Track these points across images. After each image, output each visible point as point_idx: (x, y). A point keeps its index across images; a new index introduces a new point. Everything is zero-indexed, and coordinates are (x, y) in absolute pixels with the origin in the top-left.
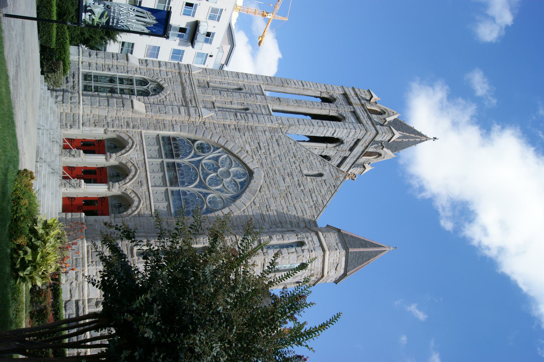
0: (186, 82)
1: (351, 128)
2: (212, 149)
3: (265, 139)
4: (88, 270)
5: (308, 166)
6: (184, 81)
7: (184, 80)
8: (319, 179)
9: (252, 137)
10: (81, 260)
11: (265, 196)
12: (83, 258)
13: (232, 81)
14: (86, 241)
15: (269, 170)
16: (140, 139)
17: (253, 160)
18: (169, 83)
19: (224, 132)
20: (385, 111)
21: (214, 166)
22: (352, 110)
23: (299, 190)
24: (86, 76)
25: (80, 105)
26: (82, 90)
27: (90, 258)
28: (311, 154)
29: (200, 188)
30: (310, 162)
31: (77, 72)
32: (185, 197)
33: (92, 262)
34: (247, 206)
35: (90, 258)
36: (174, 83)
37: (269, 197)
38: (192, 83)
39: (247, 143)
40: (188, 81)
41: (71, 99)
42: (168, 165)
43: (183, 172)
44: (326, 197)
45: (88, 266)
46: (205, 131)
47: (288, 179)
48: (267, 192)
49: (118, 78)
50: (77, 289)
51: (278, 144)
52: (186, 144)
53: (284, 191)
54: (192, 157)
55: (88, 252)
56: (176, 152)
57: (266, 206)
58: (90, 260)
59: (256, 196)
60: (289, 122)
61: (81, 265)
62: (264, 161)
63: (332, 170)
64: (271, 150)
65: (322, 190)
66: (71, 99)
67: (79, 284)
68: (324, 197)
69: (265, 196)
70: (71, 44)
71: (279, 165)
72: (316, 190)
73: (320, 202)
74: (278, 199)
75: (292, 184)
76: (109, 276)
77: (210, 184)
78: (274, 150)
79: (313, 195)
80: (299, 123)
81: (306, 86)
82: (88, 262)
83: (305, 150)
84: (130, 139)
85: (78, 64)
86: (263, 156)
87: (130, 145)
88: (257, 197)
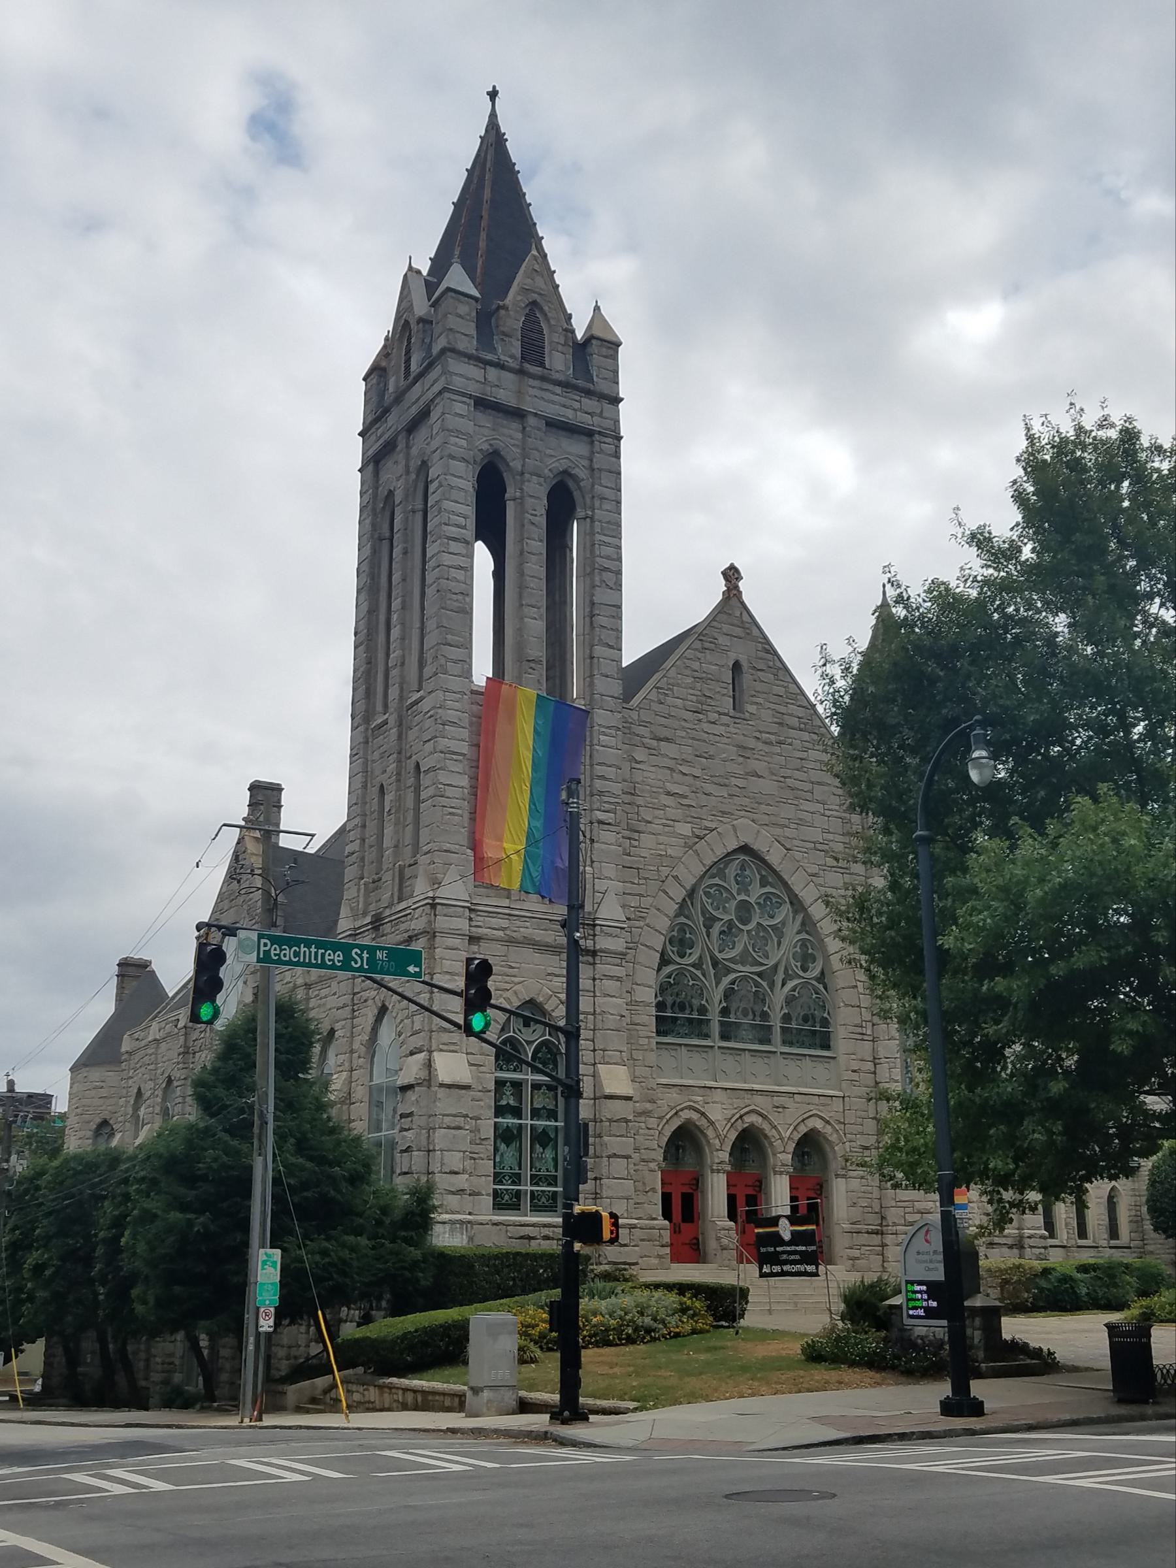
0: (503, 929)
2: (683, 920)
6: (501, 933)
7: (495, 932)
8: (747, 678)
16: (676, 1089)
18: (516, 980)
21: (724, 931)
22: (404, 433)
24: (499, 1204)
32: (669, 1006)
36: (513, 965)
38: (507, 911)
42: (725, 1037)
46: (648, 925)
47: (755, 765)
49: (497, 1120)
51: (667, 740)
52: (796, 994)
56: (818, 1025)
76: (931, 1184)
85: (482, 1224)
87: (695, 1116)
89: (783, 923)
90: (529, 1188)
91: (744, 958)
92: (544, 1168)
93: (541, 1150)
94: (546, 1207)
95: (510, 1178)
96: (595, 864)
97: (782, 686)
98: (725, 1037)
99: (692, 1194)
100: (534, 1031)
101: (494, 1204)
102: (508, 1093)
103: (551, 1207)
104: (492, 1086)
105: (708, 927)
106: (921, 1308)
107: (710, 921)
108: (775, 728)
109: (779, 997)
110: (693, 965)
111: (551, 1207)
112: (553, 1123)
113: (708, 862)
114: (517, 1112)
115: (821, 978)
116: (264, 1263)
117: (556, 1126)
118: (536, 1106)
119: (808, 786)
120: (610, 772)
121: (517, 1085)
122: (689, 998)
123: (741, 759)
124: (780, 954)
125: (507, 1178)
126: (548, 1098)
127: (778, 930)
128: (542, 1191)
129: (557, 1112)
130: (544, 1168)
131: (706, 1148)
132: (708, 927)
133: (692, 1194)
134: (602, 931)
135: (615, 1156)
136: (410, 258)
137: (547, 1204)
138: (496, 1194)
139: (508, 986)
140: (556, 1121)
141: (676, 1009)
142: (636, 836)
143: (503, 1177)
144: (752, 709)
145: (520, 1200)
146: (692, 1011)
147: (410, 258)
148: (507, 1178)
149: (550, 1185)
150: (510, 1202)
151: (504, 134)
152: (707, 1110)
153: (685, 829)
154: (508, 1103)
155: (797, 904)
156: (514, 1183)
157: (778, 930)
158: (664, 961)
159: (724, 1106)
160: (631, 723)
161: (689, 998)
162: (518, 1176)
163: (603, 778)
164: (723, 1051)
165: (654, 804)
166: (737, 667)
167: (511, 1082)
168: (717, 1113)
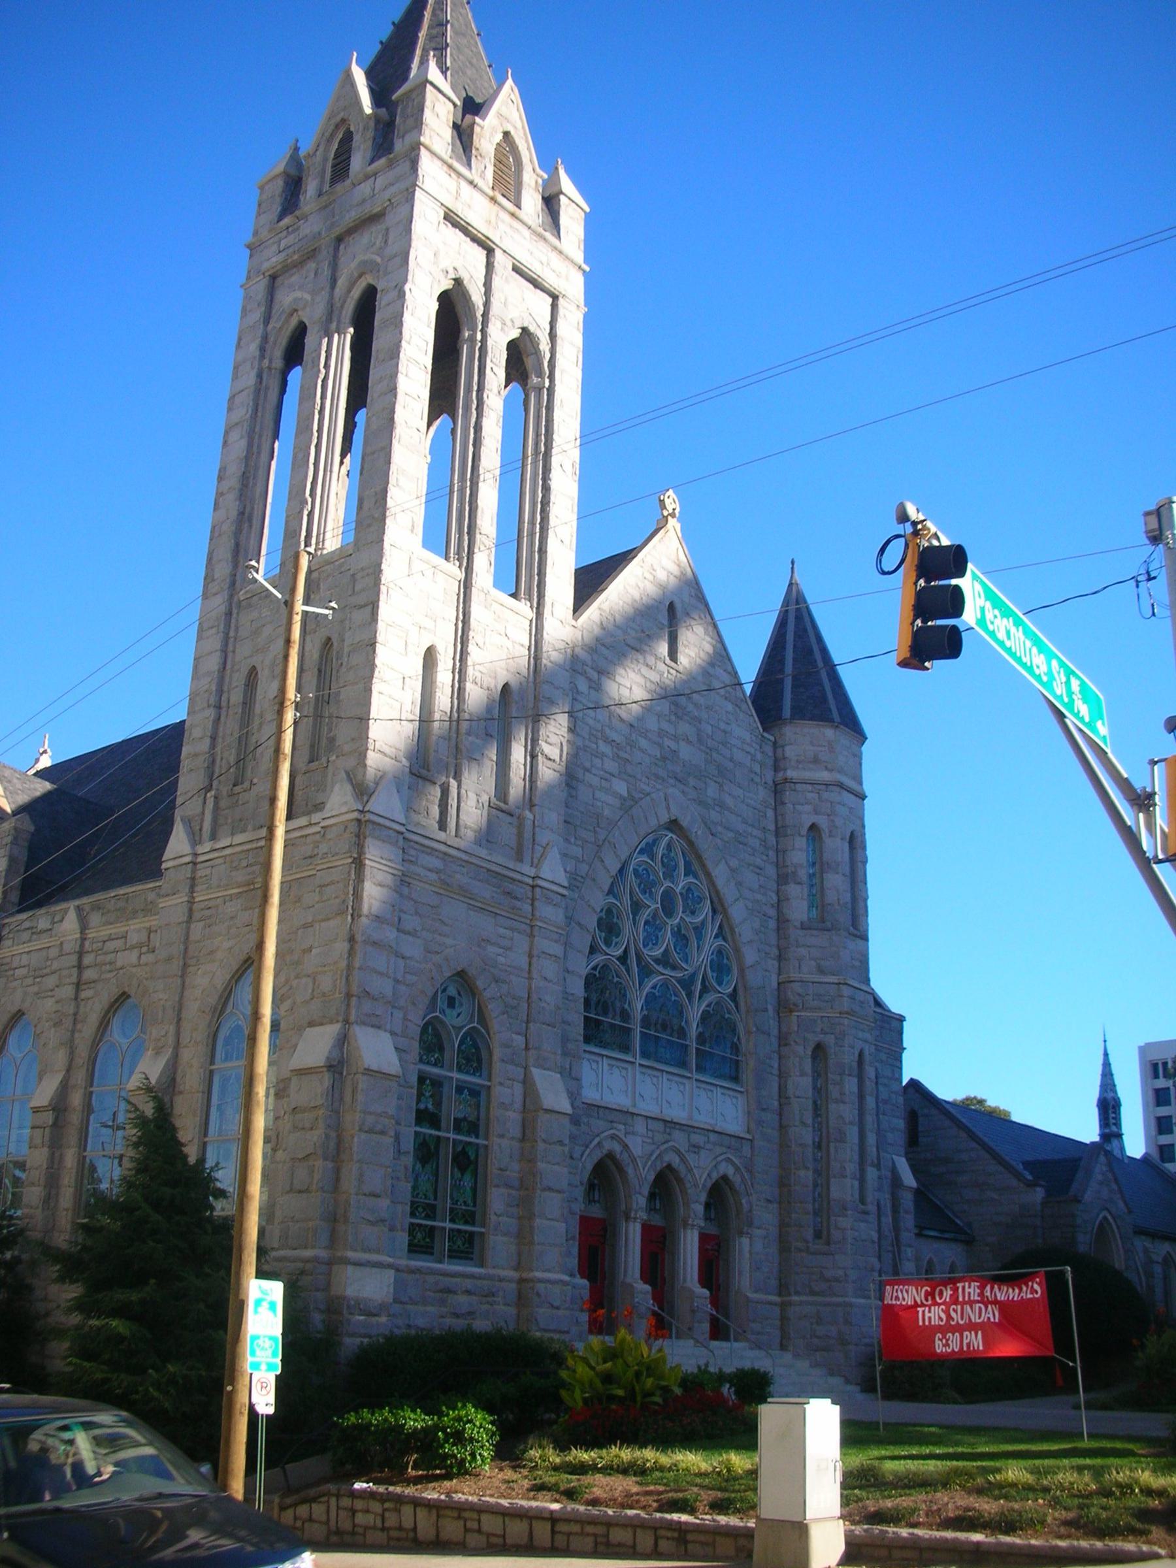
87: (617, 1148)
89: (703, 923)
90: (448, 1225)
91: (664, 960)
92: (461, 1200)
93: (460, 1176)
94: (462, 1252)
95: (424, 1209)
96: (536, 809)
98: (700, 1069)
100: (459, 1015)
101: (409, 1245)
102: (427, 1094)
103: (467, 1253)
104: (414, 1080)
105: (635, 914)
106: (972, 1327)
107: (637, 907)
109: (694, 1013)
111: (467, 1253)
112: (473, 1140)
113: (642, 833)
115: (734, 996)
116: (258, 1302)
117: (438, 1137)
121: (437, 1083)
122: (613, 999)
124: (701, 957)
125: (420, 1209)
127: (699, 930)
129: (478, 1125)
130: (461, 1200)
131: (729, 1194)
132: (635, 914)
135: (550, 1189)
136: (793, 562)
137: (462, 1248)
138: (412, 1228)
140: (477, 1137)
143: (418, 1206)
145: (432, 1240)
147: (793, 562)
148: (420, 1209)
149: (466, 1222)
150: (422, 1243)
152: (629, 1140)
153: (621, 787)
154: (426, 1107)
155: (718, 907)
156: (428, 1217)
157: (699, 930)
158: (593, 950)
161: (613, 999)
162: (433, 1208)
164: (644, 1070)
167: (430, 1079)
168: (637, 1146)
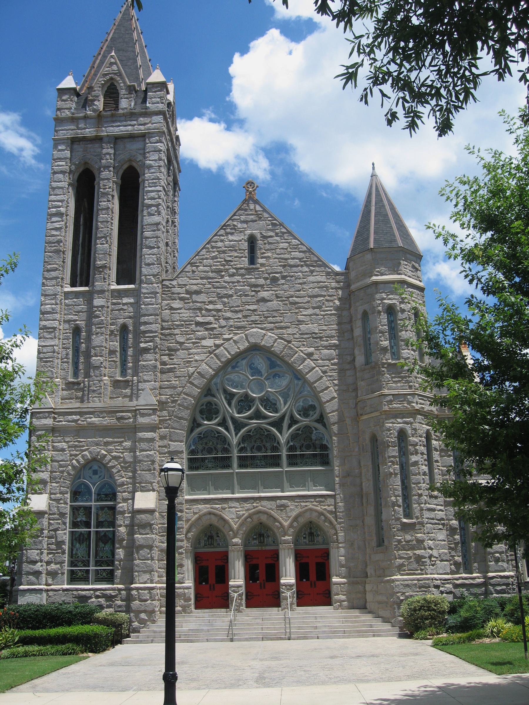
1: (157, 158)
3: (187, 311)
4: (431, 574)
5: (236, 254)
9: (185, 331)
10: (420, 582)
11: (296, 336)
12: (418, 580)
13: (61, 340)
14: (20, 585)
15: (249, 319)
17: (232, 341)
19: (178, 373)
20: (108, 77)
23: (283, 281)
25: (156, 586)
26: (113, 584)
27: (416, 572)
28: (213, 244)
29: (282, 426)
30: (229, 250)
31: (75, 593)
33: (421, 570)
34: (315, 366)
35: (416, 572)
37: (297, 330)
39: (199, 343)
40: (75, 417)
41: (146, 600)
43: (255, 447)
44: (294, 243)
45: (427, 574)
47: (264, 294)
48: (290, 331)
50: (445, 585)
53: (286, 304)
54: (227, 429)
55: (408, 574)
57: (314, 338)
58: (419, 572)
59: (297, 350)
60: (154, 264)
61: (427, 582)
62: (231, 322)
63: (243, 218)
64: (210, 307)
65: (282, 245)
66: (146, 600)
67: (443, 584)
68: (295, 248)
69: (296, 336)
70: (16, 602)
71: (235, 301)
72: (282, 256)
73: (301, 255)
74: (300, 318)
75: (273, 289)
77: (275, 410)
78: (209, 302)
79: (290, 262)
80: (154, 248)
81: (63, 210)
82: (422, 574)
83: (204, 250)
84: (299, 519)
86: (223, 322)
88: (300, 349)
93: (103, 545)
97: (287, 242)
99: (274, 564)
108: (281, 269)
110: (219, 424)
114: (88, 524)
118: (101, 519)
119: (307, 299)
120: (151, 318)
123: (253, 293)
126: (109, 514)
128: (103, 569)
133: (274, 564)
134: (140, 412)
139: (78, 453)
141: (304, 449)
142: (173, 353)
144: (261, 261)
146: (267, 450)
149: (108, 566)
151: (322, 15)
159: (237, 509)
160: (171, 288)
163: (146, 323)
165: (187, 331)
166: (252, 241)
